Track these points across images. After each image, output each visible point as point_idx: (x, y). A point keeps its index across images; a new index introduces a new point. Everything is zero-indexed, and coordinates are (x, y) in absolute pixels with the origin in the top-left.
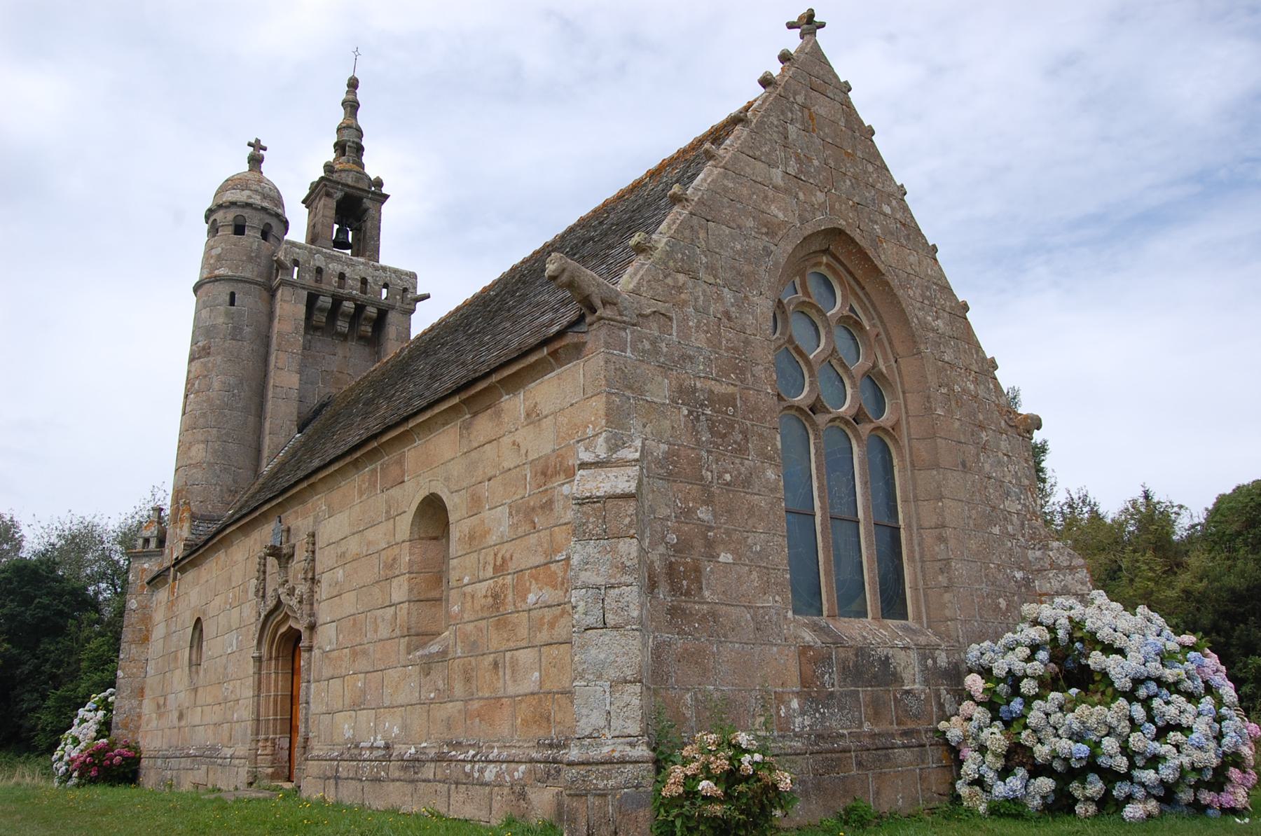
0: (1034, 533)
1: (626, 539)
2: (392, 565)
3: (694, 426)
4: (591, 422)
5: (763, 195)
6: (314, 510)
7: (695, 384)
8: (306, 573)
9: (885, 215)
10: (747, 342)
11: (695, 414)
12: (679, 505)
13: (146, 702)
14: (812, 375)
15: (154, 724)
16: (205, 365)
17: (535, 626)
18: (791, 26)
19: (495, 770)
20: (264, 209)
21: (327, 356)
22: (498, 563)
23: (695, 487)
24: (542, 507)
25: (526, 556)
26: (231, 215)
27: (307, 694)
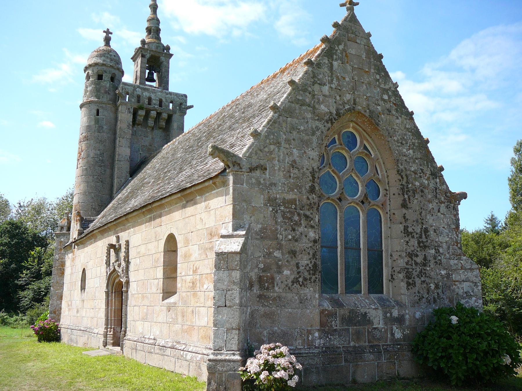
0: (454, 251)
1: (235, 271)
2: (157, 261)
3: (275, 215)
4: (227, 216)
5: (317, 100)
7: (276, 196)
11: (275, 210)
12: (266, 251)
15: (67, 313)
19: (191, 356)
22: (194, 269)
24: (210, 249)
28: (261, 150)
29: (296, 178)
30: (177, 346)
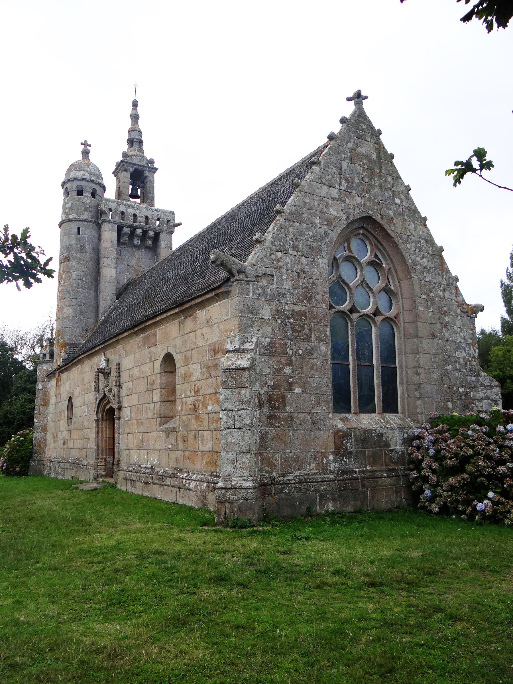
3: (284, 328)
6: (119, 352)
8: (116, 383)
9: (396, 204)
10: (313, 283)
11: (284, 322)
13: (48, 434)
14: (351, 294)
15: (52, 445)
16: (67, 265)
17: (211, 421)
18: (349, 99)
19: (194, 484)
20: (92, 181)
21: (130, 258)
23: (283, 358)
25: (207, 389)
26: (75, 184)
27: (119, 440)
28: (267, 258)
29: (305, 288)
30: (178, 474)
